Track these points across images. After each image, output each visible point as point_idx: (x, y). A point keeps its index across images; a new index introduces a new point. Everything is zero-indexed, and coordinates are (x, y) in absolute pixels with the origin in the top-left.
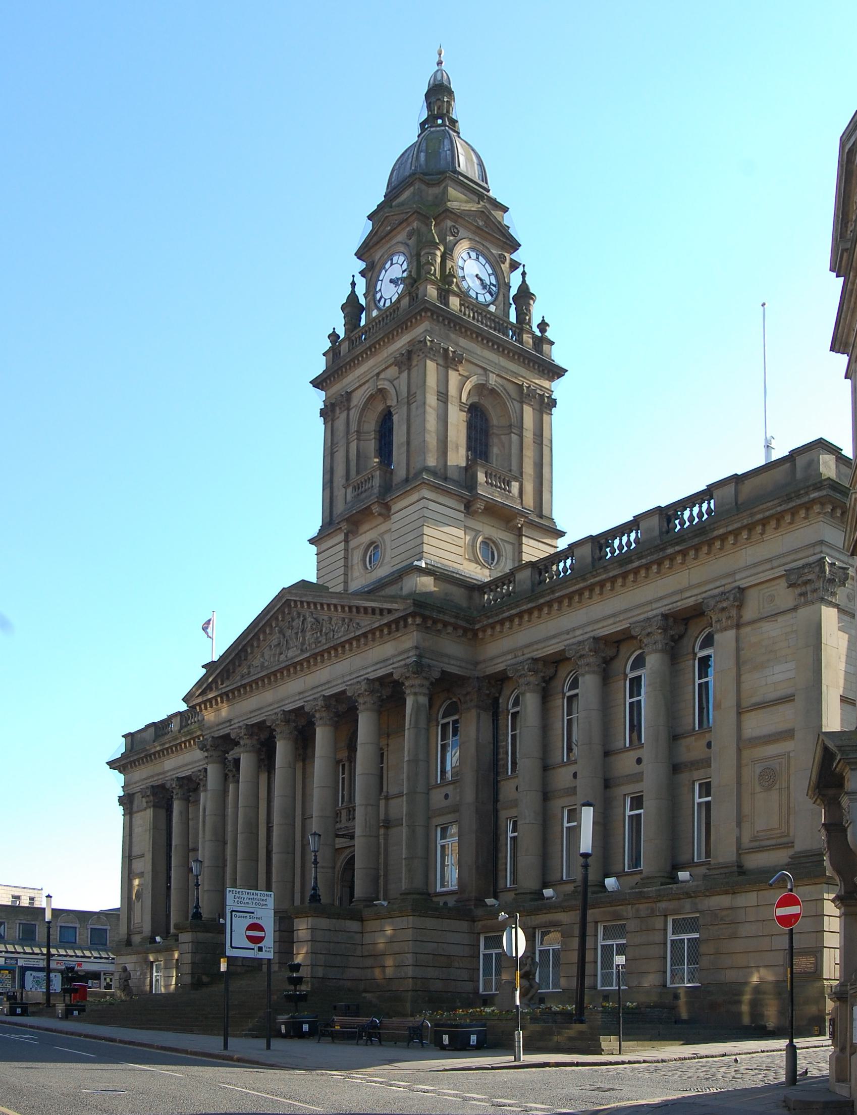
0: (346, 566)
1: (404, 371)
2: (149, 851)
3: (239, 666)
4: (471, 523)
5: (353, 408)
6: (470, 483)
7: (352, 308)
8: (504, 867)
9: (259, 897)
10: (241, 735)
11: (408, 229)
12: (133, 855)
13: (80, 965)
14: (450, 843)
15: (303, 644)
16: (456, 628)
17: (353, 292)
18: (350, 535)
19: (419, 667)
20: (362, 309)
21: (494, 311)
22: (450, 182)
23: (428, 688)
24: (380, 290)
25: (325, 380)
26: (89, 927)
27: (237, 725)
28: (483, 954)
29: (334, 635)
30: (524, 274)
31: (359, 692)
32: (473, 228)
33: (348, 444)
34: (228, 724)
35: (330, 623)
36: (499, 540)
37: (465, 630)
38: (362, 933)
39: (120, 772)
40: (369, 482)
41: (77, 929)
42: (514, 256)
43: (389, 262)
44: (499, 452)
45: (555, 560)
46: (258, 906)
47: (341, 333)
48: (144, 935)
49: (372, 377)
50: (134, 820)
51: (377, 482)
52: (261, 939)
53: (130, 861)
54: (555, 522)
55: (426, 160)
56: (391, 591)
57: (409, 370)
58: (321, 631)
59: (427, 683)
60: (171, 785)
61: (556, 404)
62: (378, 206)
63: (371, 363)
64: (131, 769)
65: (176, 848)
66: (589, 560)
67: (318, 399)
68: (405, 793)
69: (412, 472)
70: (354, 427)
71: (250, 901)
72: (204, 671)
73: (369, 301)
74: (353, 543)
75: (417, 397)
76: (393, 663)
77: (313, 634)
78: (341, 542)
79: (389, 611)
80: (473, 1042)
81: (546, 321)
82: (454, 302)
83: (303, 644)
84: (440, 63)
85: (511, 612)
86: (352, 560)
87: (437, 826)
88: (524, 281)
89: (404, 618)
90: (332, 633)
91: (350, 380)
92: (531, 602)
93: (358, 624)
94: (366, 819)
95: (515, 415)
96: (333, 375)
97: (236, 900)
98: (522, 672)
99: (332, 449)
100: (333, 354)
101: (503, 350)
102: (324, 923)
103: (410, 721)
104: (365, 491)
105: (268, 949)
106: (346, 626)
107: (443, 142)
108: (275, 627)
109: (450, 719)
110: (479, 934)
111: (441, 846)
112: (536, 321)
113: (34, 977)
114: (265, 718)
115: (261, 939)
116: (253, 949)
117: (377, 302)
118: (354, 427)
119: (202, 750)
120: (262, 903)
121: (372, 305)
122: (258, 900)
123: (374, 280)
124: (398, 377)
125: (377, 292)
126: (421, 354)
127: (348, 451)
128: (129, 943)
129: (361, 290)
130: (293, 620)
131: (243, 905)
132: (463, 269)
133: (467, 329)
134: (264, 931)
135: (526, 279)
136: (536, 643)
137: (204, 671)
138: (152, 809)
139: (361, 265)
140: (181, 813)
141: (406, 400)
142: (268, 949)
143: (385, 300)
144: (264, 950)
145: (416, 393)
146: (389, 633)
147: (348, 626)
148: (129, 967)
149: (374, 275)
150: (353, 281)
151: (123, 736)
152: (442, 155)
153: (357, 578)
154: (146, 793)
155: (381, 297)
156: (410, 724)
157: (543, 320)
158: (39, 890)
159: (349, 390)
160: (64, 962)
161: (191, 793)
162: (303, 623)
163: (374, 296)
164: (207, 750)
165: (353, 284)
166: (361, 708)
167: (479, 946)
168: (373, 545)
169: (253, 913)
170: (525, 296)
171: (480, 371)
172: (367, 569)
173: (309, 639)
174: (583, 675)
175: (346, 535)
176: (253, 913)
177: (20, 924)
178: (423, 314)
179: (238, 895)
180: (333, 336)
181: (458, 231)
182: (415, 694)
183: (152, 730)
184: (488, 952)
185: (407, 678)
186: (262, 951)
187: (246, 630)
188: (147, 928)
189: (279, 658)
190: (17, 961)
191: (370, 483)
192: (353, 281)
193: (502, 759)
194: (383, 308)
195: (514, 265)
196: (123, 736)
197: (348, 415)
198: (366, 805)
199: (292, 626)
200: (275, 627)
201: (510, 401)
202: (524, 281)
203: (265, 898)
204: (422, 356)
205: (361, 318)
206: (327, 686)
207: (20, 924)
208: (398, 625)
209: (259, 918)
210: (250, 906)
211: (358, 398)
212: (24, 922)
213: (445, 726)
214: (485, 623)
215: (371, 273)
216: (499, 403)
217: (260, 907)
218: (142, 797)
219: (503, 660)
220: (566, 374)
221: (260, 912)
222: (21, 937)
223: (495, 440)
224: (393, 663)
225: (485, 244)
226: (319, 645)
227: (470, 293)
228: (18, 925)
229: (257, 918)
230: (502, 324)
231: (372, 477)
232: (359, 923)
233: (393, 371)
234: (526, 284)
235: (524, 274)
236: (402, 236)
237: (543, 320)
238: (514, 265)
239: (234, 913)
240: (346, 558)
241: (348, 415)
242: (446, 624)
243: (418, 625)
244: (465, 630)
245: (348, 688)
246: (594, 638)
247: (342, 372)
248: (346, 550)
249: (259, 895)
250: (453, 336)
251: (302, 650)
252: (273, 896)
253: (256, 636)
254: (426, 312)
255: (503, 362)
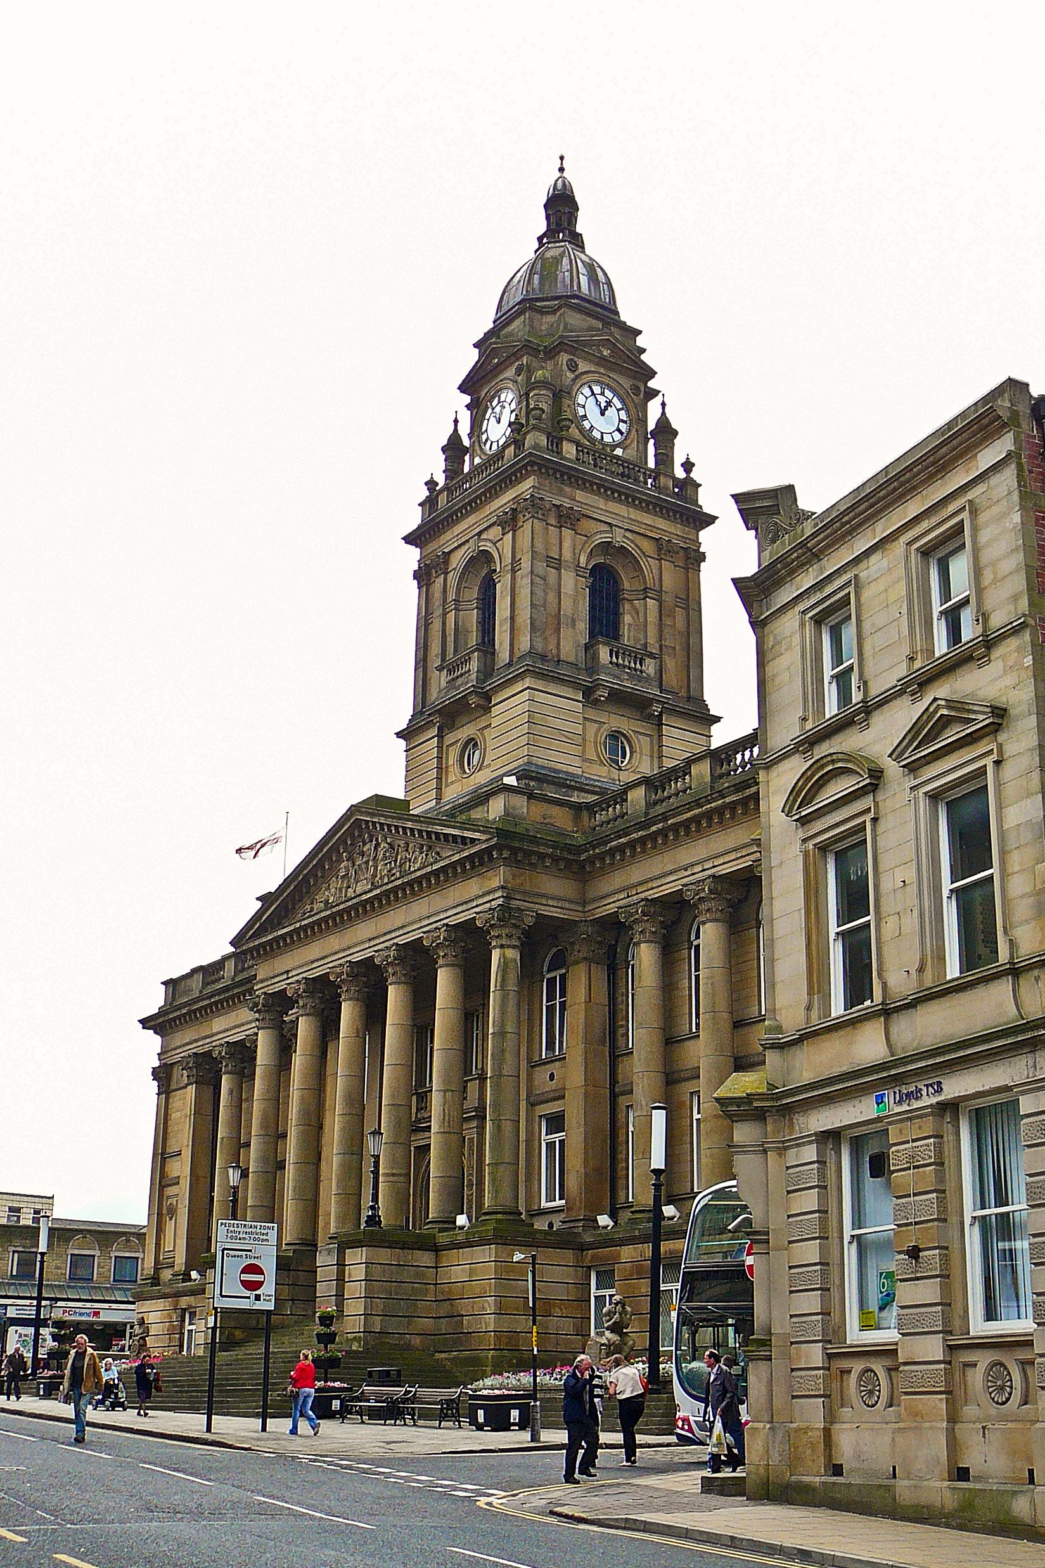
0: (439, 768)
1: (508, 532)
2: (188, 1146)
3: (300, 901)
4: (592, 714)
5: (451, 571)
6: (592, 666)
7: (454, 449)
8: (624, 1172)
9: (258, 1231)
10: (300, 993)
11: (517, 364)
12: (168, 1150)
13: (96, 1314)
14: (557, 1140)
15: (374, 876)
16: (555, 860)
17: (456, 430)
18: (446, 731)
19: (506, 913)
20: (466, 450)
21: (620, 454)
22: (566, 310)
23: (519, 938)
24: (486, 431)
25: (419, 537)
26: (113, 1255)
27: (296, 978)
28: (595, 1297)
29: (410, 866)
30: (663, 405)
31: (438, 942)
32: (598, 360)
33: (444, 615)
34: (285, 976)
35: (407, 850)
36: (632, 733)
37: (569, 863)
38: (436, 1267)
39: (156, 1033)
40: (466, 665)
41: (96, 1258)
42: (651, 384)
43: (497, 399)
44: (631, 621)
45: (672, 776)
46: (256, 1242)
47: (441, 480)
48: (176, 1268)
49: (472, 537)
50: (171, 1100)
51: (474, 665)
52: (258, 1285)
53: (164, 1160)
54: (707, 705)
55: (540, 283)
56: (476, 814)
57: (514, 531)
58: (396, 861)
59: (518, 933)
60: (220, 1053)
61: (705, 558)
62: (485, 334)
63: (472, 519)
64: (169, 1031)
65: (222, 1143)
66: (708, 779)
67: (413, 554)
68: (489, 1076)
69: (517, 654)
70: (451, 596)
71: (247, 1236)
72: (259, 904)
73: (474, 442)
74: (449, 739)
75: (522, 565)
76: (477, 906)
77: (386, 864)
78: (433, 737)
79: (473, 840)
80: (515, 1419)
81: (691, 460)
82: (569, 450)
83: (374, 876)
84: (561, 170)
85: (620, 841)
86: (447, 759)
87: (540, 1117)
88: (663, 413)
89: (488, 851)
90: (408, 863)
91: (448, 540)
92: (642, 830)
93: (438, 853)
94: (444, 1110)
95: (651, 575)
96: (428, 531)
97: (230, 1235)
98: (637, 917)
99: (426, 620)
100: (428, 504)
101: (634, 501)
102: (384, 1255)
103: (496, 980)
104: (462, 675)
105: (268, 1298)
106: (424, 855)
107: (562, 262)
108: (343, 853)
109: (557, 974)
110: (589, 1268)
111: (547, 1143)
112: (679, 459)
113: (20, 1336)
114: (328, 970)
115: (258, 1285)
116: (249, 1298)
117: (482, 445)
118: (451, 596)
119: (252, 1010)
120: (262, 1237)
121: (477, 448)
122: (257, 1234)
123: (479, 418)
124: (502, 539)
125: (483, 434)
126: (526, 514)
127: (444, 624)
128: (155, 1280)
129: (464, 430)
130: (364, 844)
131: (238, 1241)
132: (584, 407)
133: (585, 481)
134: (241, 1281)
135: (666, 411)
136: (651, 880)
137: (259, 904)
138: (194, 1085)
139: (467, 399)
140: (231, 1092)
141: (510, 566)
142: (268, 1298)
143: (492, 443)
144: (262, 1299)
145: (521, 559)
146: (473, 868)
147: (427, 855)
148: (151, 1318)
149: (480, 412)
150: (456, 418)
151: (162, 983)
152: (559, 278)
153: (452, 783)
154: (188, 1063)
155: (487, 440)
156: (496, 987)
157: (688, 458)
158: (49, 1198)
159: (446, 551)
160: (73, 1310)
161: (245, 1064)
162: (375, 848)
163: (479, 437)
164: (258, 1011)
165: (456, 421)
166: (441, 962)
167: (590, 1284)
168: (471, 743)
169: (250, 1251)
170: (666, 433)
171: (607, 528)
172: (465, 772)
173: (381, 870)
174: (704, 923)
175: (440, 729)
176: (250, 1251)
177: (14, 1252)
178: (529, 468)
179: (231, 1229)
180: (431, 484)
181: (577, 365)
182: (502, 946)
183: (199, 977)
184: (601, 1293)
185: (492, 926)
186: (260, 1300)
187: (307, 856)
188: (180, 1259)
189: (346, 891)
190: (6, 1309)
191: (468, 666)
192: (456, 418)
193: (622, 1026)
194: (488, 452)
195: (654, 393)
196: (162, 983)
197: (445, 579)
198: (445, 1091)
199: (363, 851)
200: (343, 853)
201: (644, 559)
202: (663, 413)
203: (265, 1232)
204: (528, 516)
205: (464, 461)
206: (401, 932)
207: (14, 1252)
208: (479, 863)
209: (258, 1258)
210: (247, 1242)
211: (458, 561)
212: (21, 1249)
213: (551, 982)
214: (591, 852)
215: (478, 409)
216: (630, 562)
217: (260, 1243)
218: (183, 1069)
219: (615, 899)
220: (717, 521)
221: (259, 1250)
222: (14, 1273)
223: (627, 606)
224: (477, 906)
225: (612, 376)
226: (393, 878)
227: (593, 433)
228: (11, 1254)
229: (254, 1257)
230: (633, 469)
231: (470, 658)
232: (432, 1255)
233: (496, 531)
234: (666, 417)
235: (663, 405)
236: (510, 373)
237: (688, 458)
238: (654, 393)
239: (226, 1252)
240: (439, 758)
241: (445, 579)
242: (543, 857)
243: (504, 858)
244: (569, 863)
245: (425, 935)
246: (714, 876)
247: (434, 532)
248: (440, 747)
249: (259, 1227)
250: (568, 489)
251: (372, 884)
252: (276, 1228)
253: (320, 865)
254: (532, 466)
255: (634, 514)
